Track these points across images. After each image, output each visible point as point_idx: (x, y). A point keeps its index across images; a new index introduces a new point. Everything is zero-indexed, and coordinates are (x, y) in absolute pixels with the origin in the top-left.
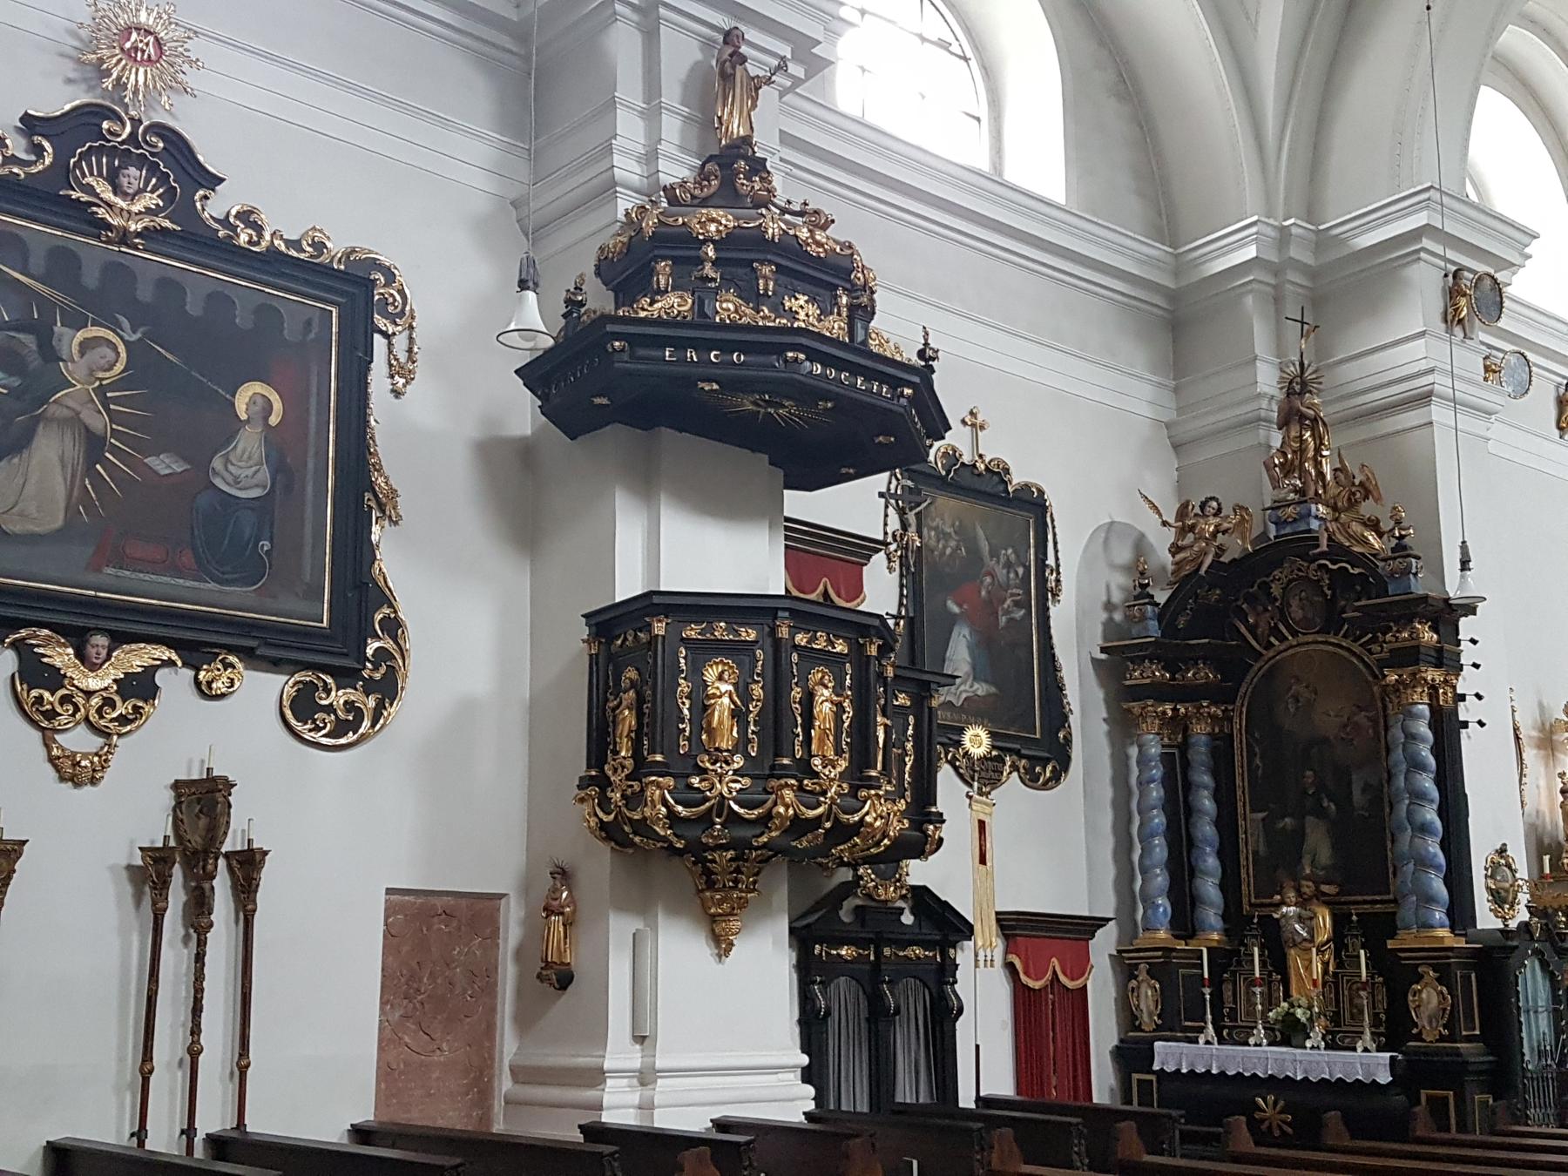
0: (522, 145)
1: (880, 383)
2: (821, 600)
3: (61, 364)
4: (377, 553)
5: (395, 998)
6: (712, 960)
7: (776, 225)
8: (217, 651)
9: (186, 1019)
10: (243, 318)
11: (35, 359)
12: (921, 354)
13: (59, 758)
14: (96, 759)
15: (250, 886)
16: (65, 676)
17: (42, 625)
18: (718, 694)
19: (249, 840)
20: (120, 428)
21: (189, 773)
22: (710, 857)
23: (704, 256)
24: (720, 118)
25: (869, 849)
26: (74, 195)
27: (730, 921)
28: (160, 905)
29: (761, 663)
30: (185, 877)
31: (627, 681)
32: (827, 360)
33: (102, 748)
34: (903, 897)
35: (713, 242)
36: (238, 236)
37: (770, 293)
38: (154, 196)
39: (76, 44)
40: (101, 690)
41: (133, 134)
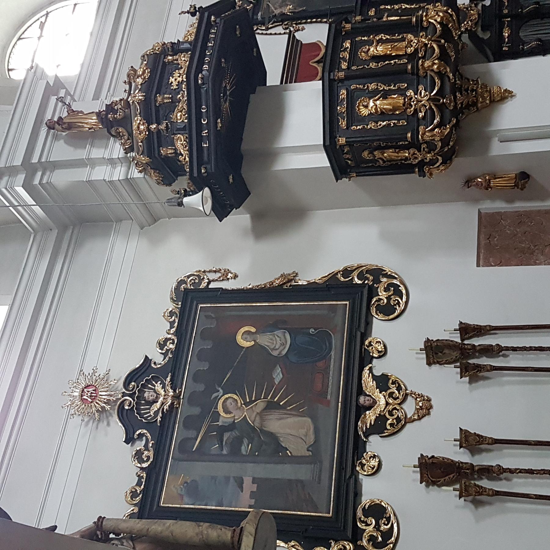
0: (114, 225)
1: (210, 33)
2: (322, 64)
3: (236, 421)
4: (311, 282)
5: (533, 259)
6: (514, 100)
7: (137, 95)
8: (363, 349)
9: (545, 354)
10: (208, 345)
11: (235, 433)
12: (193, 14)
13: (419, 416)
14: (418, 399)
15: (478, 329)
16: (379, 414)
17: (356, 425)
18: (375, 107)
19: (455, 330)
20: (263, 395)
21: (423, 359)
22: (460, 106)
23: (156, 130)
24: (90, 129)
25: (454, 20)
26: (159, 419)
27: (493, 92)
28: (489, 368)
29: (357, 86)
30: (473, 358)
31: (369, 155)
32: (201, 62)
33: (413, 397)
34: (476, 5)
35: (148, 126)
36: (171, 348)
37: (170, 96)
38: (156, 385)
39: (91, 422)
40: (385, 398)
41: (130, 396)
